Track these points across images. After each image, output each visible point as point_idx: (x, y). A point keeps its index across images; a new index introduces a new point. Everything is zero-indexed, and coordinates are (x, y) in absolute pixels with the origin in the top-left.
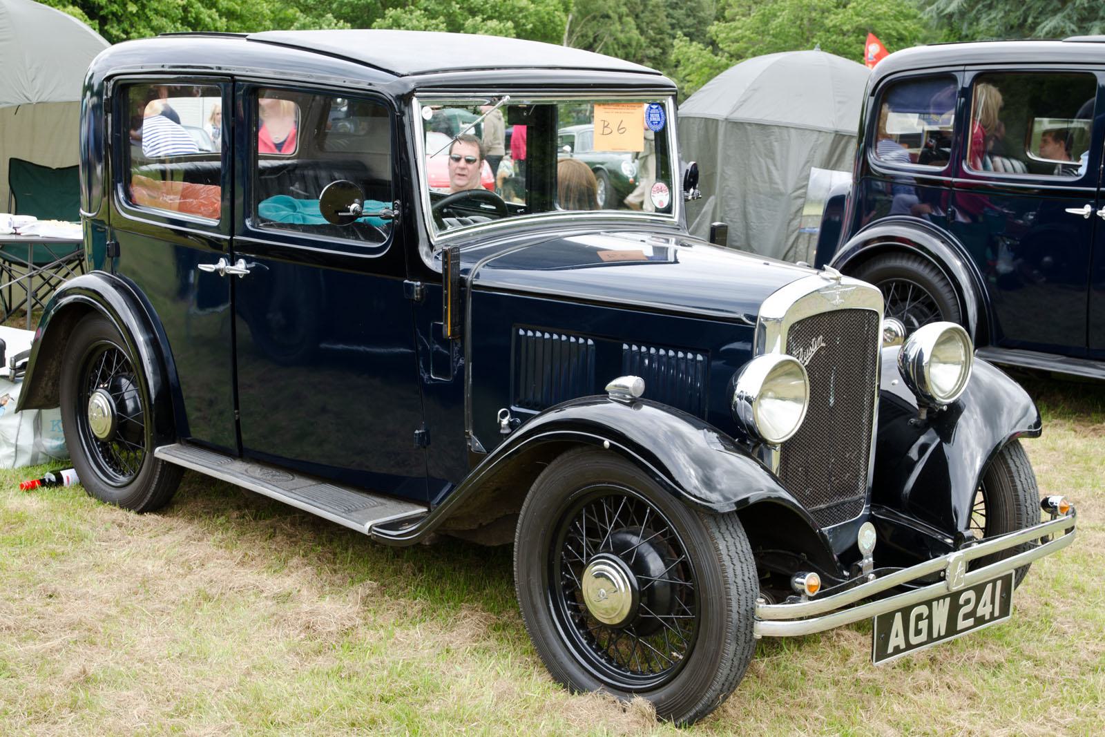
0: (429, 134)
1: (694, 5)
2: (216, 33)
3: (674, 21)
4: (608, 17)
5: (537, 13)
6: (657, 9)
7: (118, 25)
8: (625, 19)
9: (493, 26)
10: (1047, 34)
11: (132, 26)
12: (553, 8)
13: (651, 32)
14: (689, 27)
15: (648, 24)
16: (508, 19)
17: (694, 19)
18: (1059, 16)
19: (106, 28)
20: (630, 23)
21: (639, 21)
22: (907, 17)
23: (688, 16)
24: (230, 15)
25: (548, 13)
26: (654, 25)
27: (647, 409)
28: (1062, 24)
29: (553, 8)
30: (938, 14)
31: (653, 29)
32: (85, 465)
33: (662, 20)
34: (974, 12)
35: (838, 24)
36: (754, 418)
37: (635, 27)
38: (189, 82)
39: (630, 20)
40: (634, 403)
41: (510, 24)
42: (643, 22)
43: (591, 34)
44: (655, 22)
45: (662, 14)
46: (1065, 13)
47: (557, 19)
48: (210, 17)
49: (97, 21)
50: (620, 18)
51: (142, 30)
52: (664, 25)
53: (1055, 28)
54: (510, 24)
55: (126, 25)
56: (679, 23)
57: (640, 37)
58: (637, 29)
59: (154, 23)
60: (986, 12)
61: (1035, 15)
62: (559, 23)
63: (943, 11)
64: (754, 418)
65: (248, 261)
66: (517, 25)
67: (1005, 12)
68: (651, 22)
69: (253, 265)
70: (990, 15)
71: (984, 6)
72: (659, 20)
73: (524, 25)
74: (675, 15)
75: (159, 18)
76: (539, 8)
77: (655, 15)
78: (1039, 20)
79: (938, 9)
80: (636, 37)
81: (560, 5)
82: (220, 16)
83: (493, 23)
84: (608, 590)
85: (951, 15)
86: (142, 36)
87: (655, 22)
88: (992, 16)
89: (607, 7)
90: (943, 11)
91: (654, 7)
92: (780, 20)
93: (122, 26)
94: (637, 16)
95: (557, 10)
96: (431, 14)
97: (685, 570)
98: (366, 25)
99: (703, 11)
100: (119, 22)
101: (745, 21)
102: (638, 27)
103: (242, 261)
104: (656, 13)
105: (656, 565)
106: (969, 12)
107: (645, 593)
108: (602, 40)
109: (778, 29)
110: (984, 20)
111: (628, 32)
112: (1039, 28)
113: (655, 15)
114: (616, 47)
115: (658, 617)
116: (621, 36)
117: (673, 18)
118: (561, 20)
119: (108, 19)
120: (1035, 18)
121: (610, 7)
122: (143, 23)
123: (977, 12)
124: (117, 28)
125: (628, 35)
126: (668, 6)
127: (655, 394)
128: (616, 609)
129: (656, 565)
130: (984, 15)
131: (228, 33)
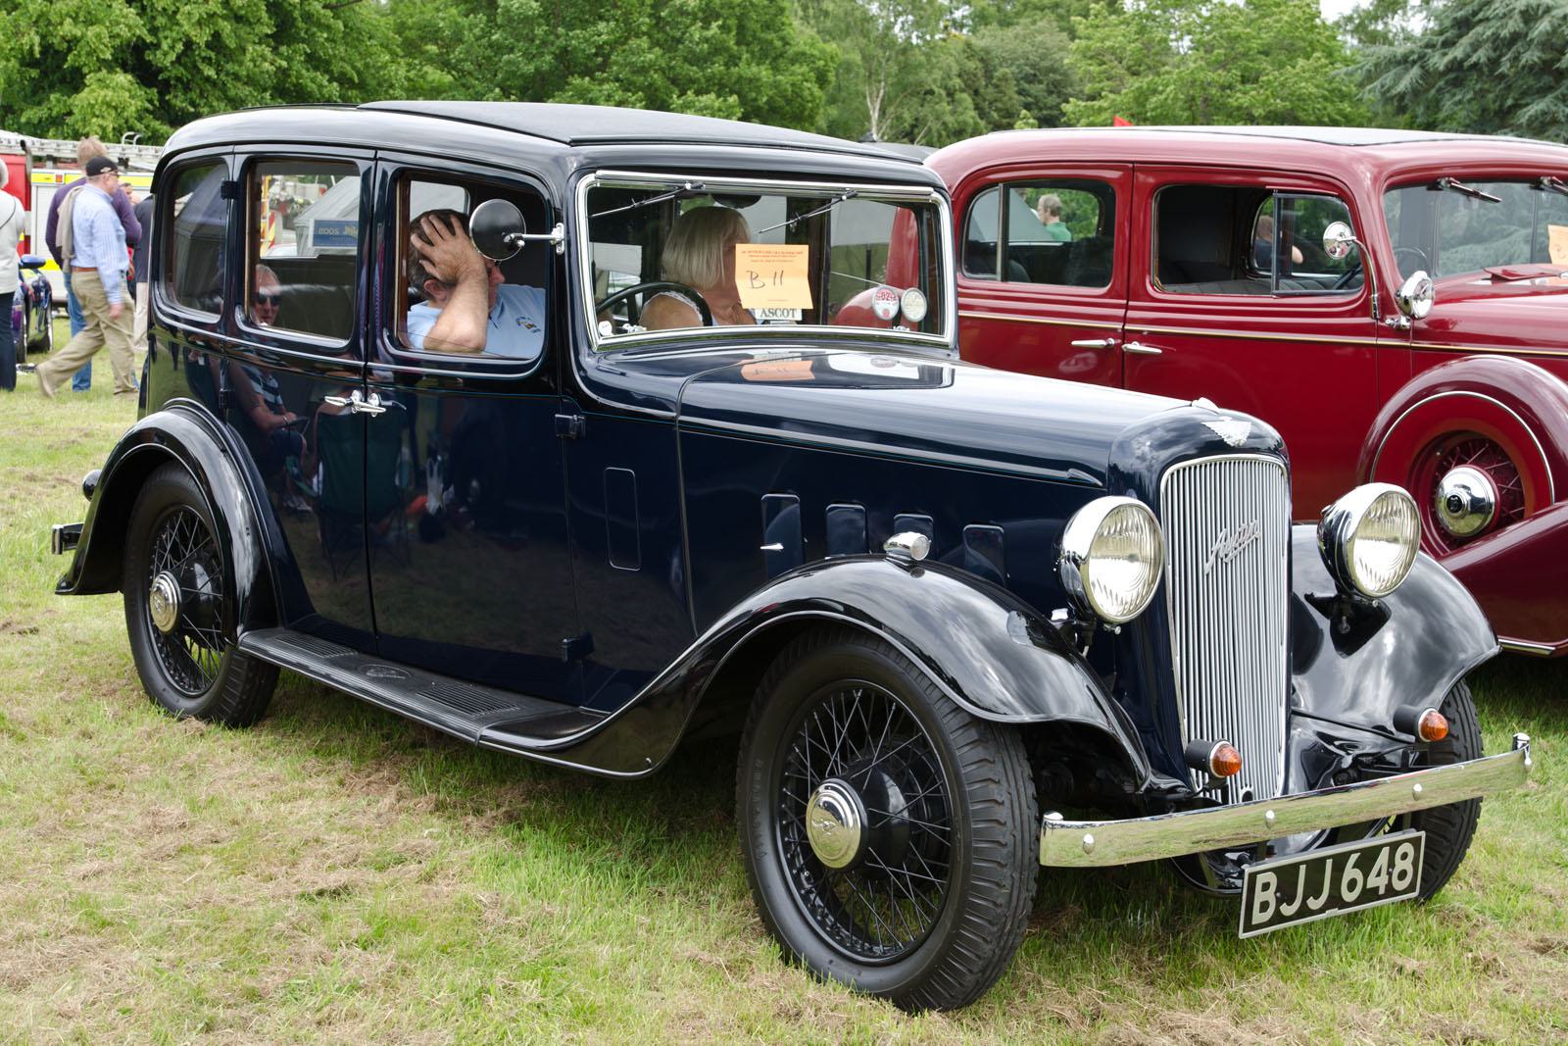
0: (893, 210)
1: (1059, 77)
2: (328, 102)
3: (1030, 99)
4: (931, 92)
5: (776, 85)
6: (1003, 83)
7: (185, 93)
8: (958, 96)
9: (709, 102)
10: (1531, 121)
11: (201, 96)
12: (800, 77)
13: (995, 115)
14: (1050, 108)
15: (991, 103)
16: (732, 93)
17: (1059, 97)
18: (1550, 97)
19: (167, 98)
20: (965, 100)
21: (979, 100)
22: (1343, 97)
23: (1050, 93)
24: (343, 80)
25: (793, 85)
26: (999, 105)
27: (930, 577)
28: (1554, 109)
29: (800, 77)
30: (1383, 94)
31: (997, 110)
32: (147, 646)
33: (1011, 99)
34: (1433, 91)
35: (1246, 105)
36: (1084, 588)
37: (972, 106)
38: (322, 165)
39: (966, 99)
40: (913, 567)
41: (733, 99)
42: (985, 100)
43: (906, 115)
44: (1001, 101)
45: (1011, 90)
46: (1558, 93)
47: (806, 93)
48: (313, 80)
49: (155, 90)
50: (950, 94)
51: (215, 104)
52: (1012, 106)
53: (1544, 113)
54: (733, 99)
55: (194, 95)
56: (1036, 103)
57: (979, 120)
58: (975, 109)
59: (232, 93)
60: (1448, 92)
61: (1516, 96)
62: (809, 98)
63: (1389, 90)
64: (1084, 588)
65: (385, 396)
66: (743, 101)
67: (1475, 93)
68: (996, 101)
69: (389, 403)
70: (1454, 95)
71: (1447, 83)
72: (1006, 99)
73: (755, 100)
74: (1032, 92)
75: (239, 85)
76: (779, 77)
77: (1001, 92)
78: (1523, 102)
79: (1382, 86)
80: (971, 121)
81: (812, 74)
82: (330, 81)
83: (709, 99)
84: (837, 820)
85: (1402, 96)
86: (214, 112)
87: (1001, 101)
88: (1457, 98)
89: (929, 80)
90: (1389, 90)
91: (999, 80)
92: (1162, 97)
93: (189, 96)
94: (976, 92)
95: (807, 81)
96: (627, 86)
97: (937, 803)
98: (539, 98)
99: (1071, 86)
100: (187, 89)
101: (1114, 100)
102: (977, 107)
103: (375, 395)
104: (1003, 89)
105: (896, 798)
106: (1427, 90)
107: (878, 831)
108: (925, 125)
109: (1159, 111)
110: (1449, 103)
111: (962, 114)
112: (1520, 112)
113: (1001, 92)
114: (944, 133)
115: (888, 869)
116: (949, 119)
117: (1030, 96)
118: (812, 94)
119: (170, 86)
120: (1516, 100)
121: (935, 81)
122: (218, 93)
123: (1438, 91)
124: (181, 97)
125: (961, 118)
126: (1022, 78)
127: (944, 557)
128: (1557, 98)
129: (896, 798)
130: (1447, 96)
131: (346, 102)
